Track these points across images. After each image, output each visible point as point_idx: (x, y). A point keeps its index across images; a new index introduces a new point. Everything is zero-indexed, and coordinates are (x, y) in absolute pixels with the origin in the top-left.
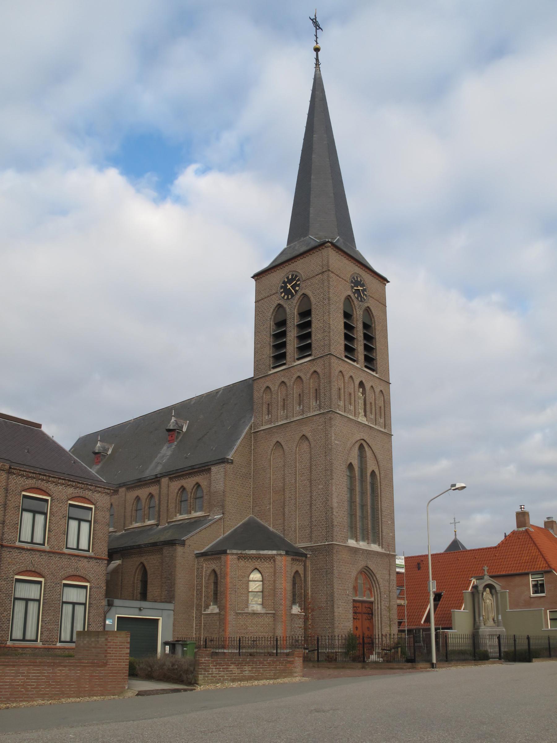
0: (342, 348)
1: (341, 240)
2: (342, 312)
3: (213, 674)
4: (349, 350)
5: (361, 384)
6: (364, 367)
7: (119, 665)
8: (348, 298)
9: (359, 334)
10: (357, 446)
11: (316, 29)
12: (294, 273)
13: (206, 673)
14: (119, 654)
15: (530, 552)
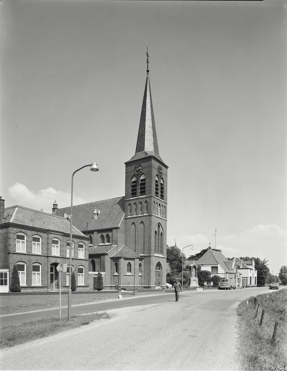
0: (155, 192)
4: (157, 193)
5: (160, 205)
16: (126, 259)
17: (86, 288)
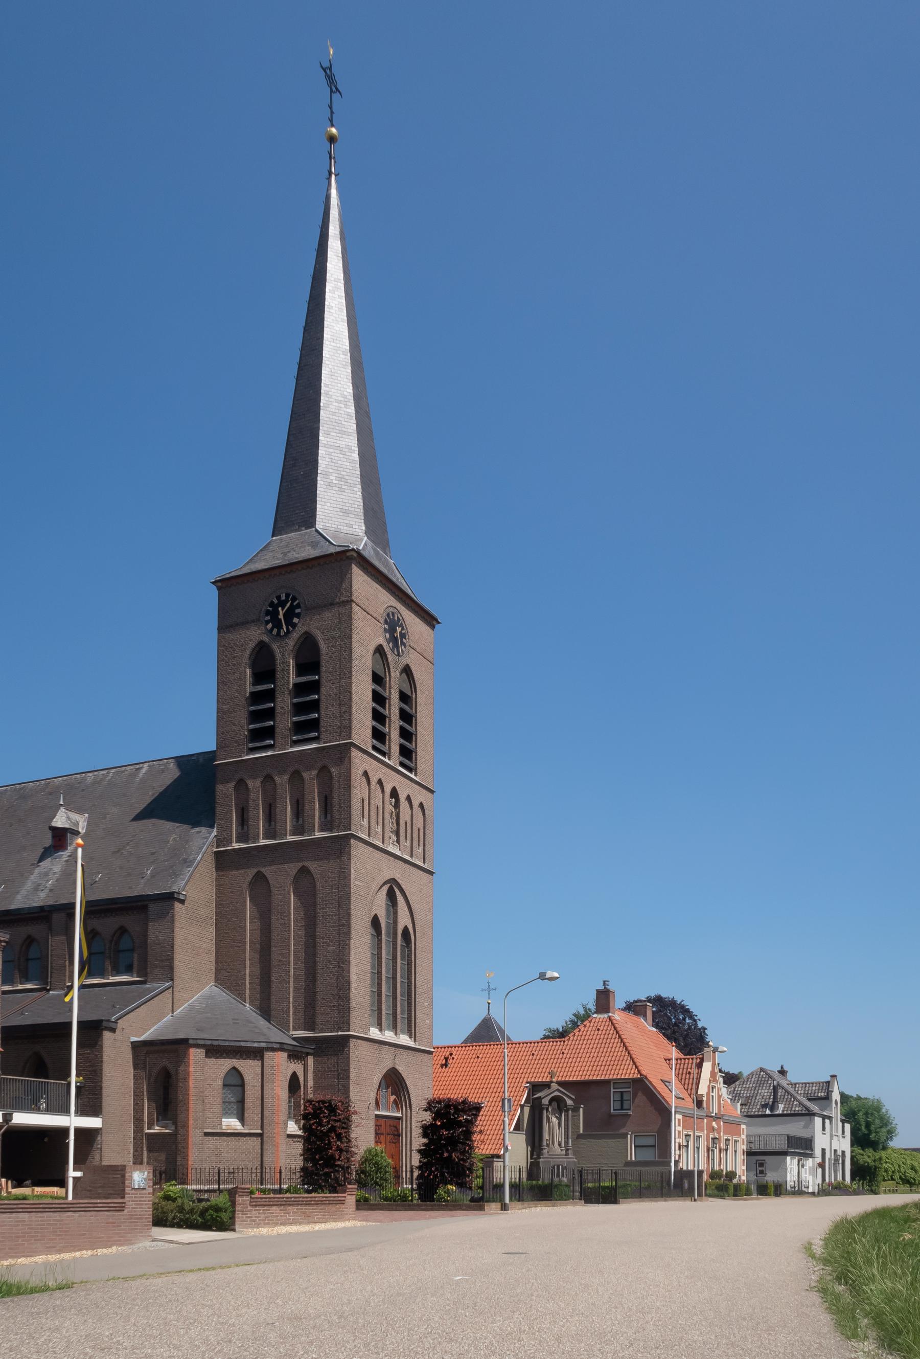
0: (369, 732)
1: (370, 543)
2: (370, 673)
3: (252, 1217)
4: (379, 735)
5: (394, 793)
6: (398, 765)
7: (140, 1208)
8: (379, 650)
9: (393, 709)
10: (385, 889)
11: (332, 91)
12: (289, 591)
13: (244, 1216)
14: (140, 1194)
15: (613, 1050)
16: (215, 1051)
17: (408, 825)
